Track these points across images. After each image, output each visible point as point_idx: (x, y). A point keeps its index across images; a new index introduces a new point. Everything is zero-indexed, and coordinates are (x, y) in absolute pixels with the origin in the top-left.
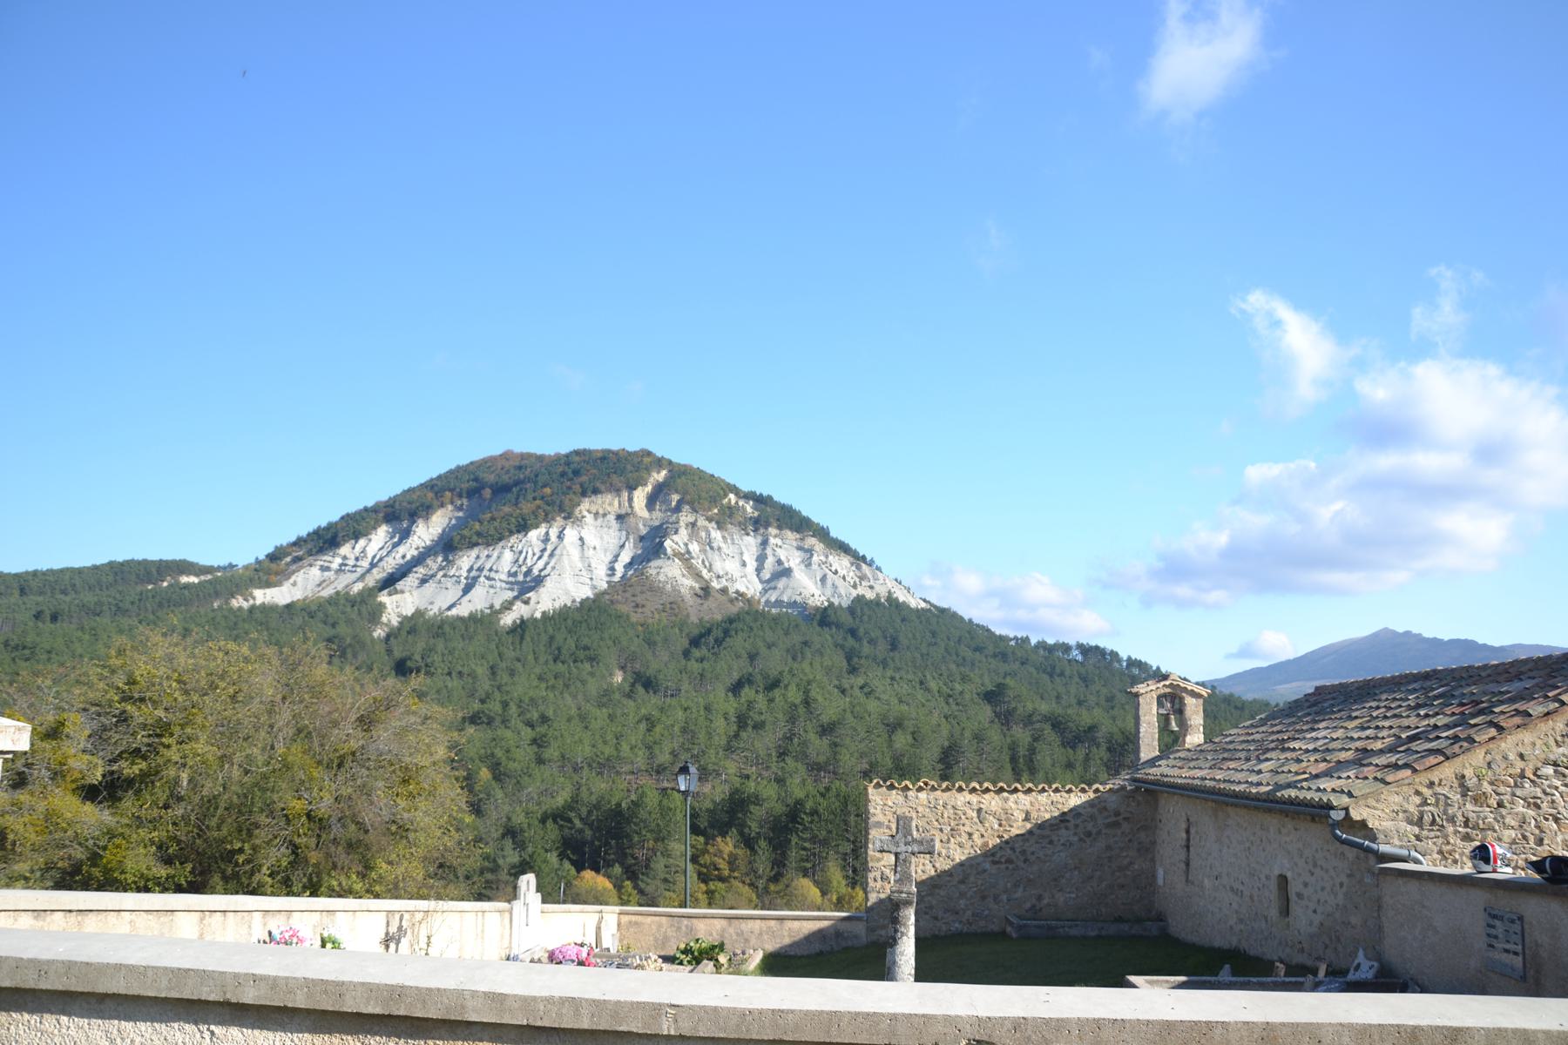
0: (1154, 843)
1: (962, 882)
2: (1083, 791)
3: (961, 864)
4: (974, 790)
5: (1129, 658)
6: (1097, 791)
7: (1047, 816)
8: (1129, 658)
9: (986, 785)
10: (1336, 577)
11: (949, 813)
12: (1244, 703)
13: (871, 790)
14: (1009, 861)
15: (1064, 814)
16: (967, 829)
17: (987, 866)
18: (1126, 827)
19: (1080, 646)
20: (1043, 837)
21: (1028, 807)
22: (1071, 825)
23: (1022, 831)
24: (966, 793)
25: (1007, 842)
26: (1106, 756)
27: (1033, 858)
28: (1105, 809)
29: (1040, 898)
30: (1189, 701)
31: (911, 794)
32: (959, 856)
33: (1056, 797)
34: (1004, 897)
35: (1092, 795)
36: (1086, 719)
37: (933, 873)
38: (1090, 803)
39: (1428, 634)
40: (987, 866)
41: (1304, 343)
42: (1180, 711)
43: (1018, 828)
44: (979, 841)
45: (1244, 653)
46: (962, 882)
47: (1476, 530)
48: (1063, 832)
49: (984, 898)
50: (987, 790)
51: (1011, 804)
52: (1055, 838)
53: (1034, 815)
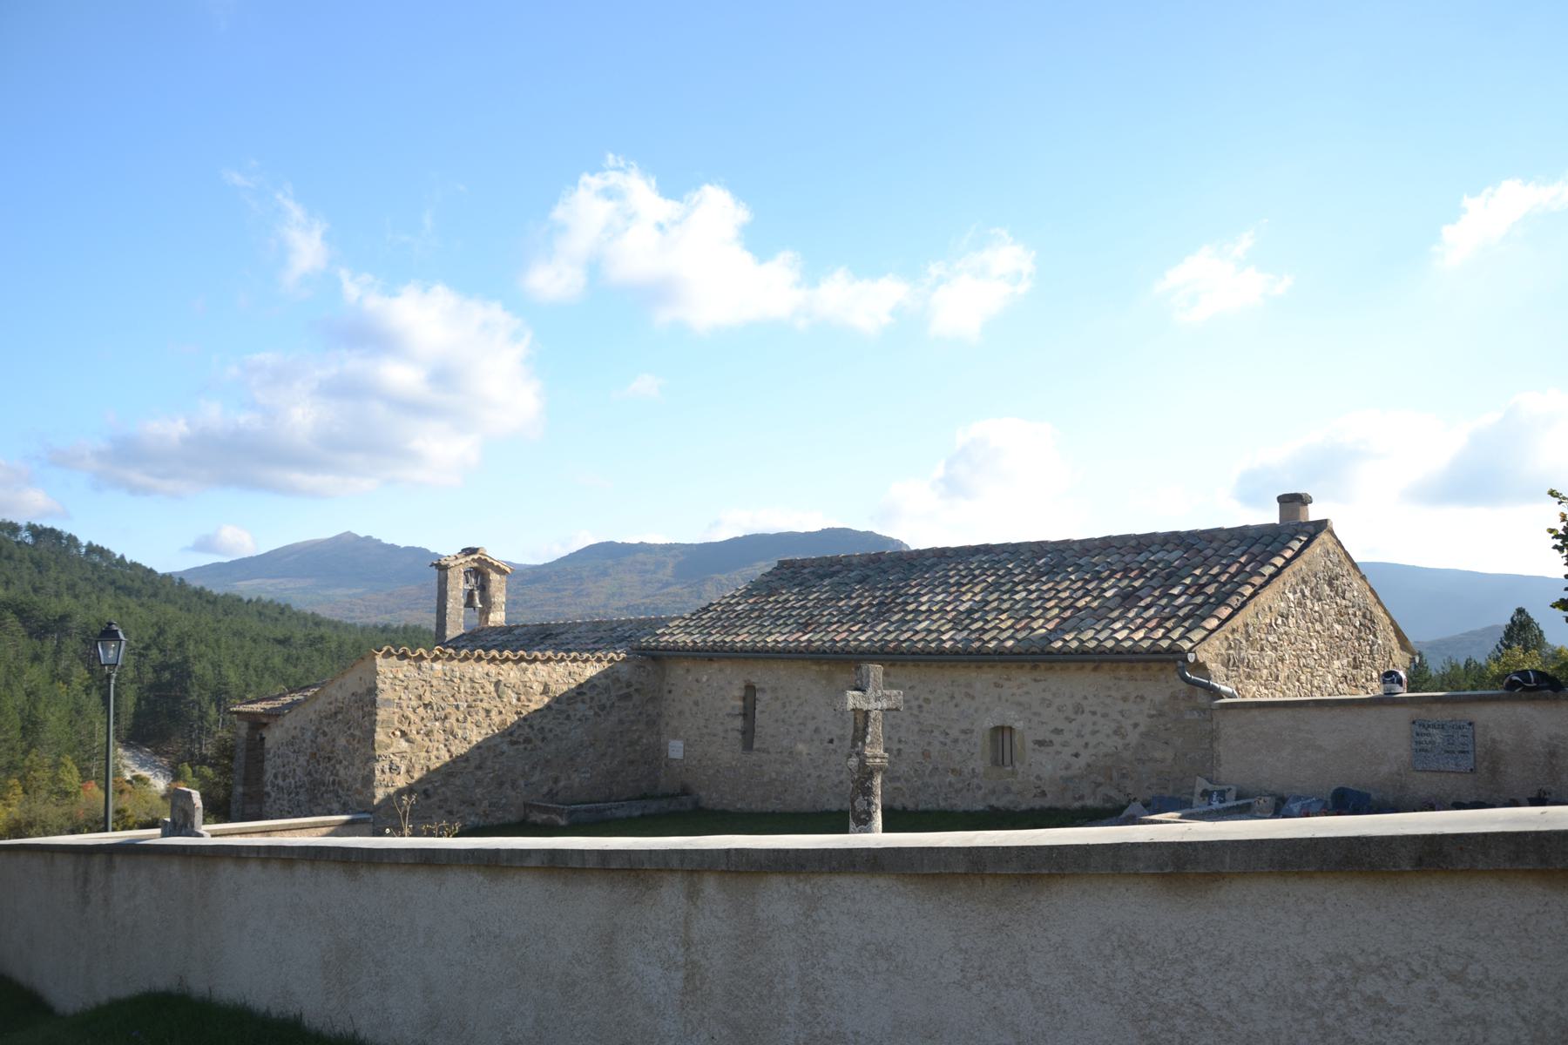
0: (659, 715)
1: (479, 767)
2: (599, 660)
3: (478, 747)
4: (493, 659)
5: (90, 544)
6: (612, 660)
7: (565, 688)
8: (90, 544)
9: (506, 653)
10: (297, 477)
11: (465, 687)
12: (216, 598)
13: (379, 660)
14: (528, 741)
15: (581, 685)
16: (485, 705)
17: (505, 747)
18: (636, 697)
19: (32, 528)
20: (560, 712)
21: (547, 679)
22: (586, 698)
23: (540, 706)
24: (484, 663)
25: (525, 719)
26: (81, 648)
27: (550, 736)
28: (618, 679)
29: (556, 780)
30: (494, 577)
31: (425, 664)
32: (476, 737)
33: (573, 667)
34: (522, 782)
35: (606, 665)
36: (56, 607)
37: (448, 759)
38: (604, 674)
39: (387, 540)
40: (505, 747)
41: (307, 248)
42: (484, 588)
43: (538, 702)
44: (496, 719)
45: (203, 545)
46: (479, 767)
47: (441, 448)
48: (580, 706)
49: (501, 784)
50: (507, 659)
51: (529, 673)
52: (571, 713)
53: (553, 687)
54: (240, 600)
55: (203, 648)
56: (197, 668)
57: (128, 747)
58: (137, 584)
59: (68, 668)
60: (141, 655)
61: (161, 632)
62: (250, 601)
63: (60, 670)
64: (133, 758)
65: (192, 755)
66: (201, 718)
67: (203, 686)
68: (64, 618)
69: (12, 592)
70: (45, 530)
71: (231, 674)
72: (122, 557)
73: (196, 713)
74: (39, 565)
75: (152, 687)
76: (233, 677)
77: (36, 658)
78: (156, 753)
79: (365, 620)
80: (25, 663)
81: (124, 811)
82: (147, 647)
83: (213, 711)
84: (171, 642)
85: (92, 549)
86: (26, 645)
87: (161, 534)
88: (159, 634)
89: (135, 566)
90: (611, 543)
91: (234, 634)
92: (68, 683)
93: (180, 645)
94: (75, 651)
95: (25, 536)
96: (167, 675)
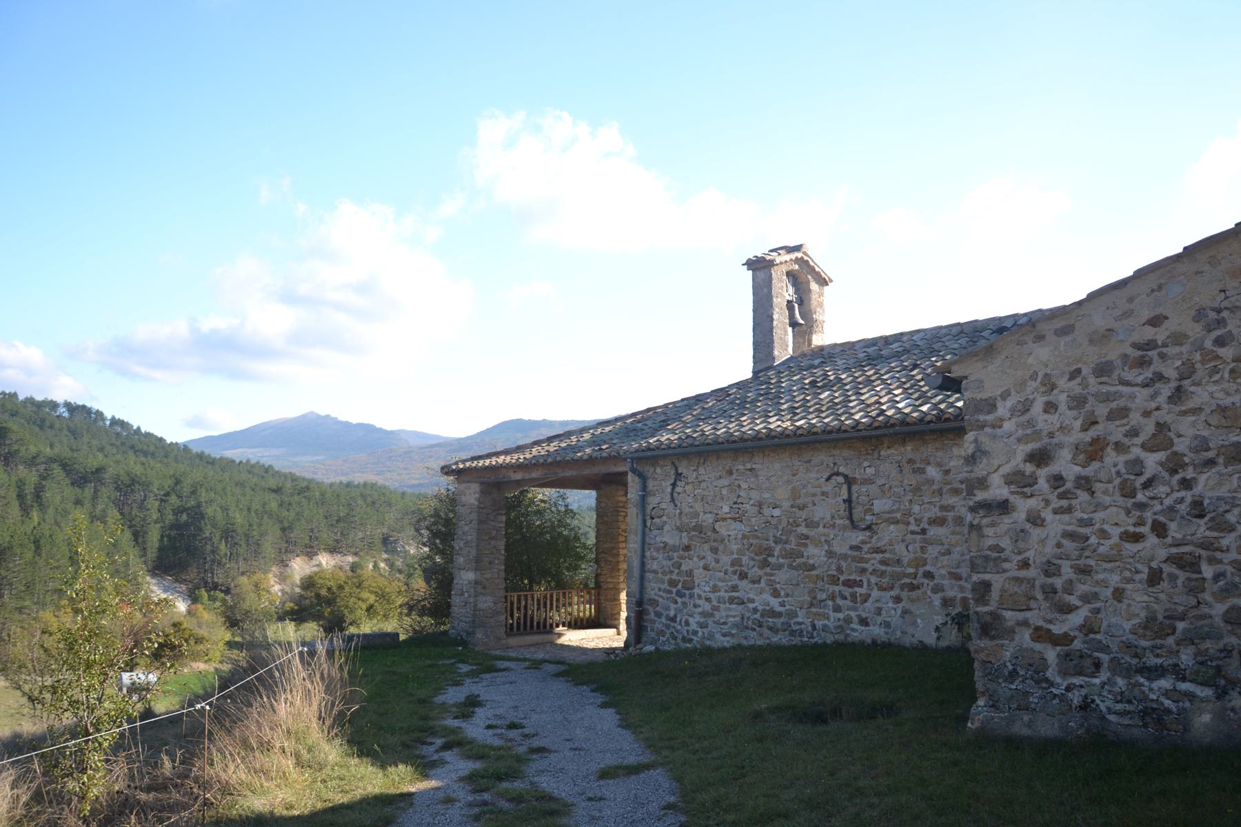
5: (113, 418)
8: (113, 418)
19: (68, 405)
36: (94, 461)
39: (342, 418)
45: (194, 422)
54: (233, 461)
55: (212, 495)
56: (210, 511)
57: (154, 575)
58: (152, 448)
59: (104, 511)
60: (162, 500)
61: (178, 482)
62: (241, 462)
63: (98, 512)
64: (158, 584)
65: (206, 583)
66: (213, 552)
67: (214, 526)
68: (99, 470)
69: (56, 450)
70: (78, 406)
71: (238, 516)
72: (139, 428)
73: (209, 547)
74: (74, 433)
75: (172, 527)
76: (239, 518)
77: (78, 502)
78: (176, 581)
79: (332, 480)
80: (70, 506)
81: (180, 624)
82: (167, 494)
83: (223, 546)
84: (186, 491)
85: (115, 422)
86: (70, 492)
87: (176, 410)
88: (176, 484)
89: (148, 435)
90: (520, 420)
91: (237, 484)
92: (105, 523)
93: (193, 492)
94: (109, 498)
95: (63, 411)
96: (184, 517)
